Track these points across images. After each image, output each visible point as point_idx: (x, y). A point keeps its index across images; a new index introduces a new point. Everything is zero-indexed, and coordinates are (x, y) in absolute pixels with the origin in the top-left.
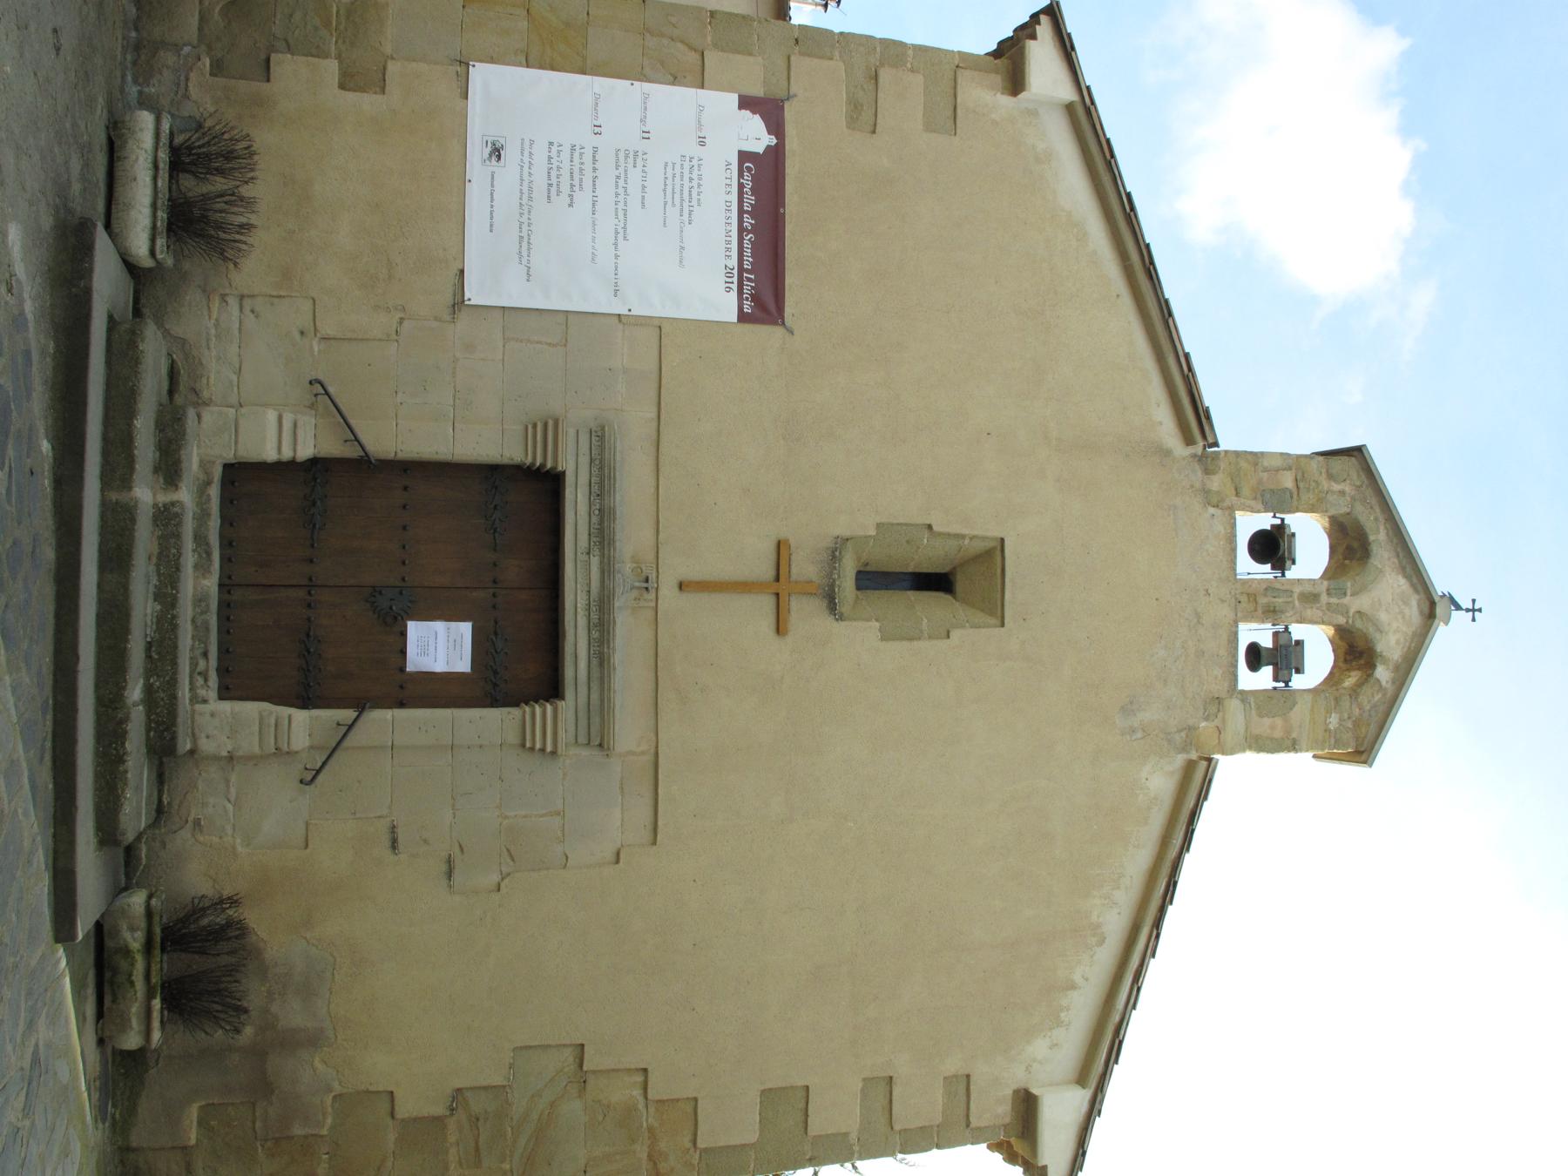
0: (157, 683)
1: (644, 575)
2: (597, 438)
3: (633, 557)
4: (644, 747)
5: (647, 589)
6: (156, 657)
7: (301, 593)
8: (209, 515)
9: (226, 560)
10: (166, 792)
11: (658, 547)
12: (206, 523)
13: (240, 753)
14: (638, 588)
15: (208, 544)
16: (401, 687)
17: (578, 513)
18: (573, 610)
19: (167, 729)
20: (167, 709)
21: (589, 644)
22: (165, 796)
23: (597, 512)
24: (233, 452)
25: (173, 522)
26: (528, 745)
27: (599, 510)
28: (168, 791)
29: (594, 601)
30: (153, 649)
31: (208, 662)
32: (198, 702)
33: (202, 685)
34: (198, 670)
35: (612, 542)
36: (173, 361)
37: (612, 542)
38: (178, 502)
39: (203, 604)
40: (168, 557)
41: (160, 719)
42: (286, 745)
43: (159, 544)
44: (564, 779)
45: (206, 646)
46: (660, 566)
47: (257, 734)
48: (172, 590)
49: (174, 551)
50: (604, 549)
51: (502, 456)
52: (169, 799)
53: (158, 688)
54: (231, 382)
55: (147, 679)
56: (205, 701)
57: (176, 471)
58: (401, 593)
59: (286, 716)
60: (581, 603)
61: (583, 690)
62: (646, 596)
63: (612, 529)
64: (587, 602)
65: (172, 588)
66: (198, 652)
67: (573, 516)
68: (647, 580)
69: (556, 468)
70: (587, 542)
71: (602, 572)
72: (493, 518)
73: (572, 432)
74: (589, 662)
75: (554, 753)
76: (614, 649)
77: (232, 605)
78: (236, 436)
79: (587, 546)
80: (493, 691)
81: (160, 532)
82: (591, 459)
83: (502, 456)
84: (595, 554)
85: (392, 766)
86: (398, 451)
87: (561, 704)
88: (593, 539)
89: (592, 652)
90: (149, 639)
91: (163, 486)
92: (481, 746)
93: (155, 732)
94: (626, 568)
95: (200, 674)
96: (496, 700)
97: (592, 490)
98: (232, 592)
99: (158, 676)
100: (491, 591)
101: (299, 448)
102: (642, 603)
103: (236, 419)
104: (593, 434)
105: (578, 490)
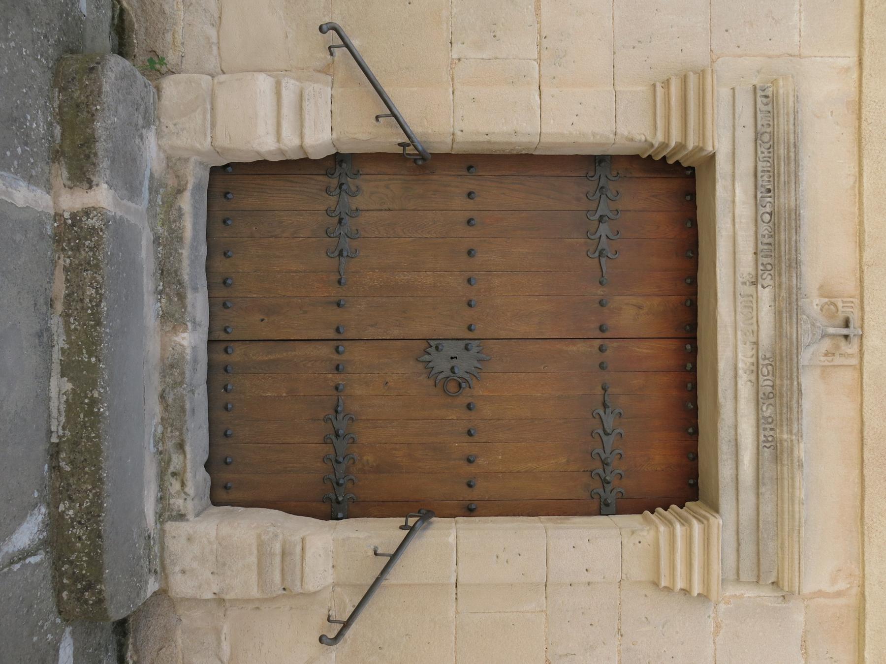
0: (71, 512)
1: (841, 316)
2: (765, 100)
3: (821, 287)
4: (841, 585)
5: (846, 337)
6: (68, 469)
7: (325, 351)
8: (180, 239)
9: (216, 306)
10: (130, 647)
11: (862, 272)
12: (176, 250)
13: (231, 596)
14: (834, 336)
15: (180, 283)
16: (470, 485)
17: (737, 220)
18: (730, 373)
19: (89, 587)
20: (88, 555)
21: (758, 427)
22: (129, 654)
23: (767, 217)
24: (209, 139)
25: (87, 243)
26: (664, 583)
27: (771, 214)
28: (134, 645)
29: (765, 359)
30: (63, 455)
31: (185, 457)
32: (171, 518)
33: (178, 492)
34: (172, 469)
35: (795, 264)
36: (122, 10)
37: (794, 265)
38: (95, 209)
39: (176, 372)
40: (82, 300)
41: (77, 571)
42: (298, 583)
43: (67, 280)
44: (716, 633)
45: (181, 434)
46: (866, 302)
47: (254, 568)
48: (90, 357)
49: (90, 292)
50: (780, 275)
51: (615, 134)
52: (135, 658)
53: (73, 520)
54: (208, 38)
55: (52, 505)
56: (181, 517)
57: (88, 157)
58: (466, 348)
59: (297, 538)
60: (745, 360)
61: (748, 498)
62: (843, 345)
63: (793, 243)
64: (754, 360)
65: (90, 354)
66: (170, 444)
67: (729, 225)
68: (847, 324)
69: (702, 149)
70: (752, 264)
71: (778, 314)
72: (598, 235)
73: (724, 92)
74: (758, 454)
75: (704, 597)
76: (800, 434)
77: (229, 368)
78: (213, 116)
79: (753, 273)
80: (601, 491)
81: (68, 261)
82: (756, 133)
83: (615, 134)
84: (765, 284)
85: (457, 612)
86: (459, 133)
87: (716, 522)
88: (762, 260)
89: (762, 438)
90: (54, 440)
91: (69, 183)
92: (589, 584)
93: (71, 592)
94: (813, 304)
95: (174, 474)
96: (607, 505)
97: (760, 183)
98: (229, 350)
99: (70, 499)
100: (597, 343)
101: (307, 131)
102: (838, 361)
103: (212, 90)
104: (759, 93)
105: (737, 185)
